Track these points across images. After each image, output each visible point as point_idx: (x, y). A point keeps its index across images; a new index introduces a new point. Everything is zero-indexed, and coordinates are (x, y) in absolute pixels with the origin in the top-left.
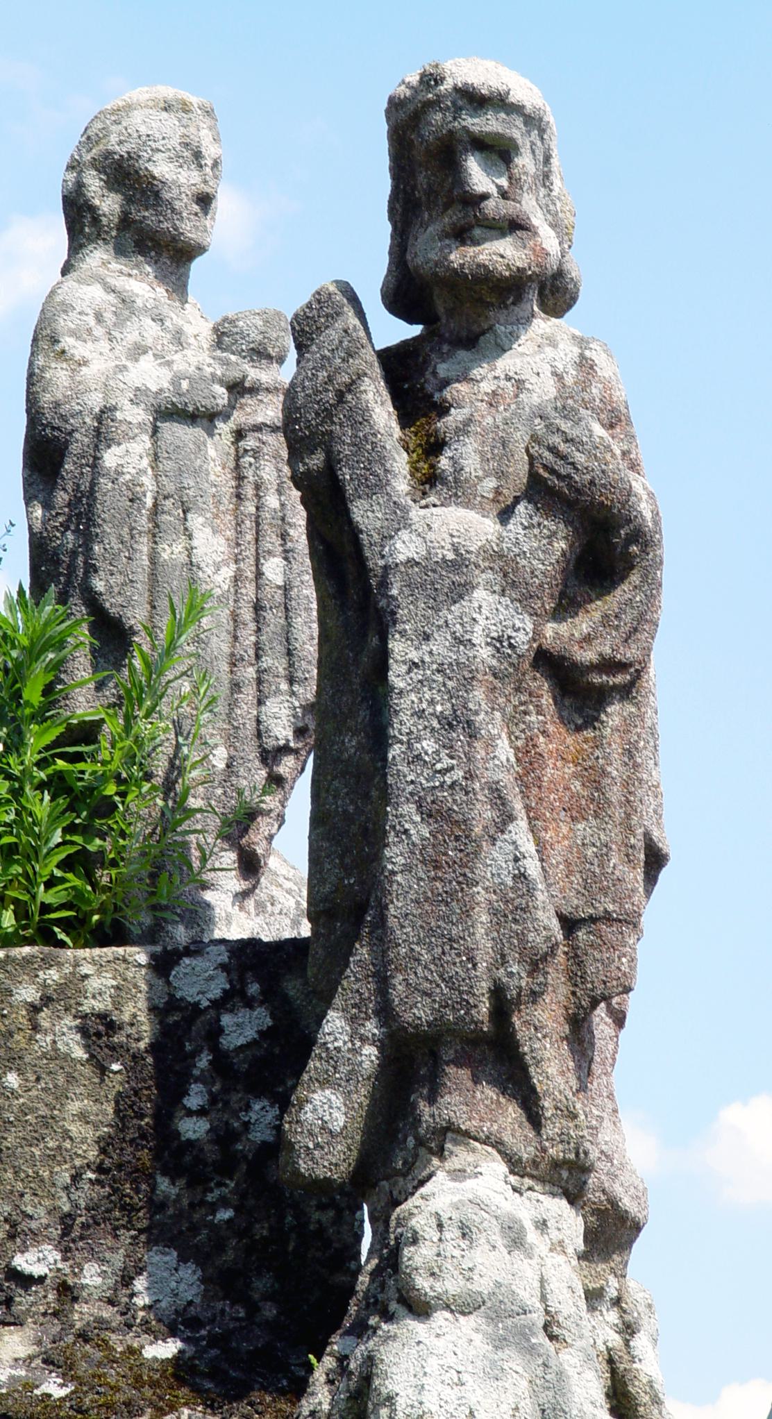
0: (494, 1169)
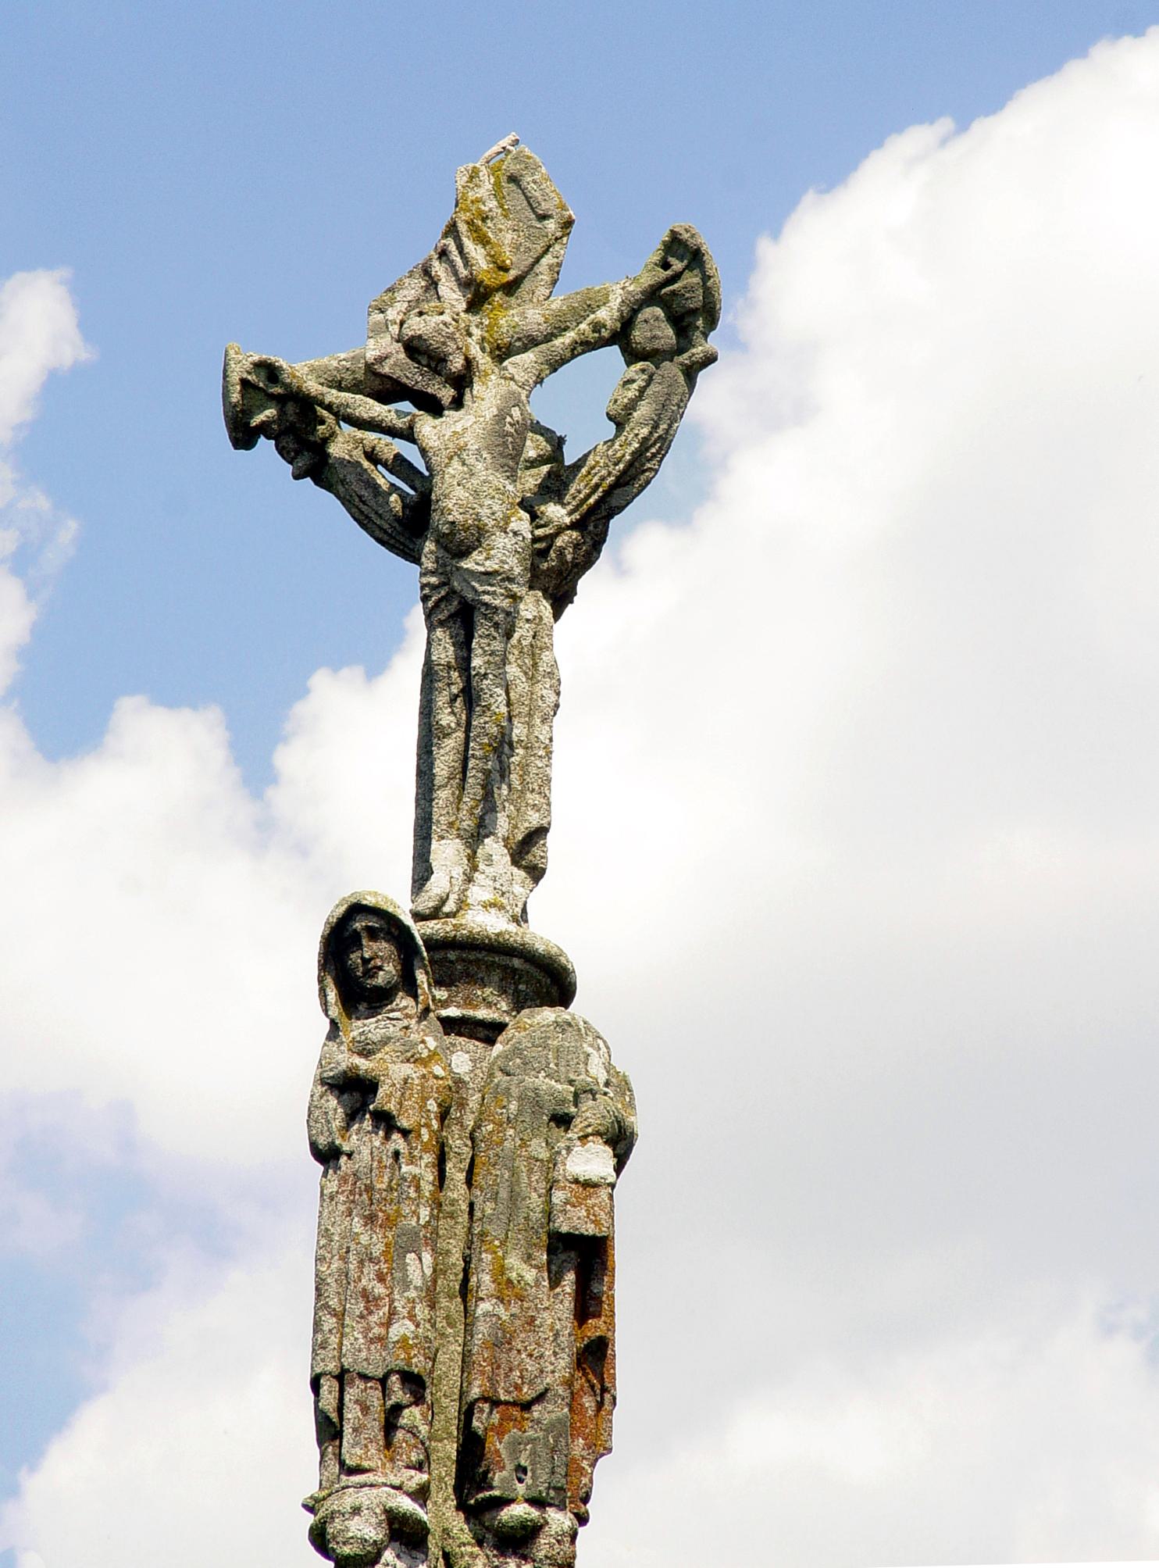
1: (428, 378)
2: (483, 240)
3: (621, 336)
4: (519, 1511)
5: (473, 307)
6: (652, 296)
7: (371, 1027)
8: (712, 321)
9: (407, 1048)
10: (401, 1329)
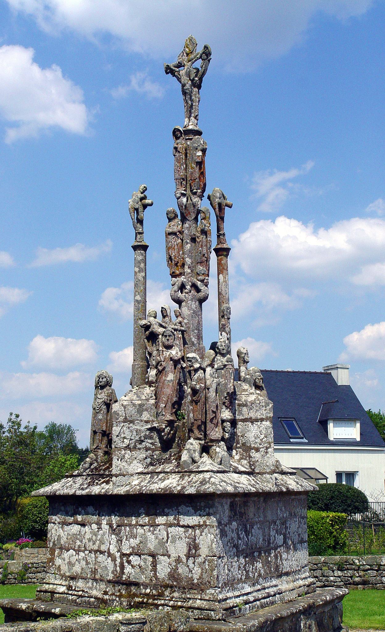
0: (192, 439)
1: (180, 65)
2: (188, 48)
3: (201, 57)
4: (195, 190)
5: (187, 56)
6: (203, 53)
7: (178, 141)
8: (211, 55)
9: (182, 143)
10: (182, 174)
